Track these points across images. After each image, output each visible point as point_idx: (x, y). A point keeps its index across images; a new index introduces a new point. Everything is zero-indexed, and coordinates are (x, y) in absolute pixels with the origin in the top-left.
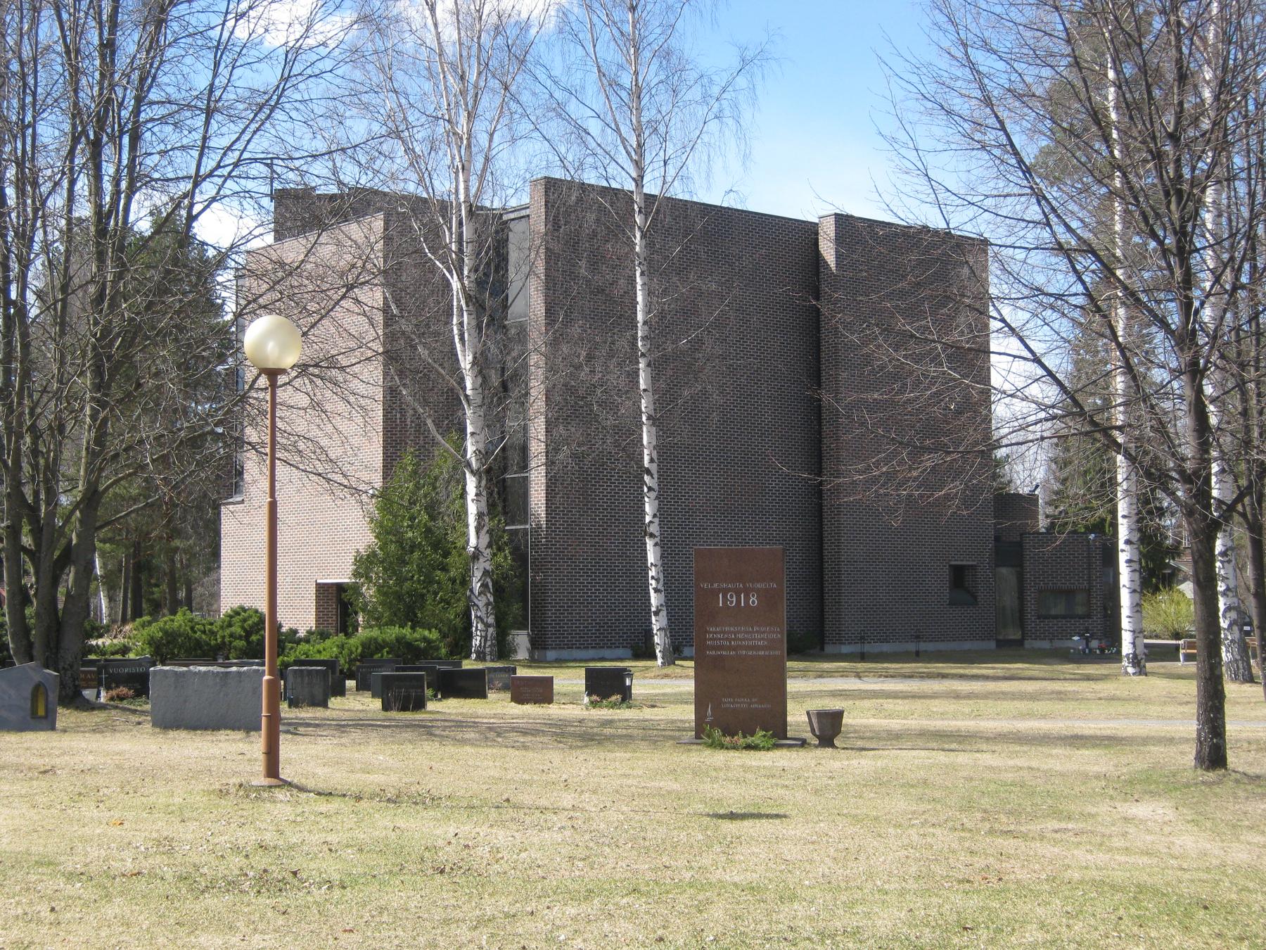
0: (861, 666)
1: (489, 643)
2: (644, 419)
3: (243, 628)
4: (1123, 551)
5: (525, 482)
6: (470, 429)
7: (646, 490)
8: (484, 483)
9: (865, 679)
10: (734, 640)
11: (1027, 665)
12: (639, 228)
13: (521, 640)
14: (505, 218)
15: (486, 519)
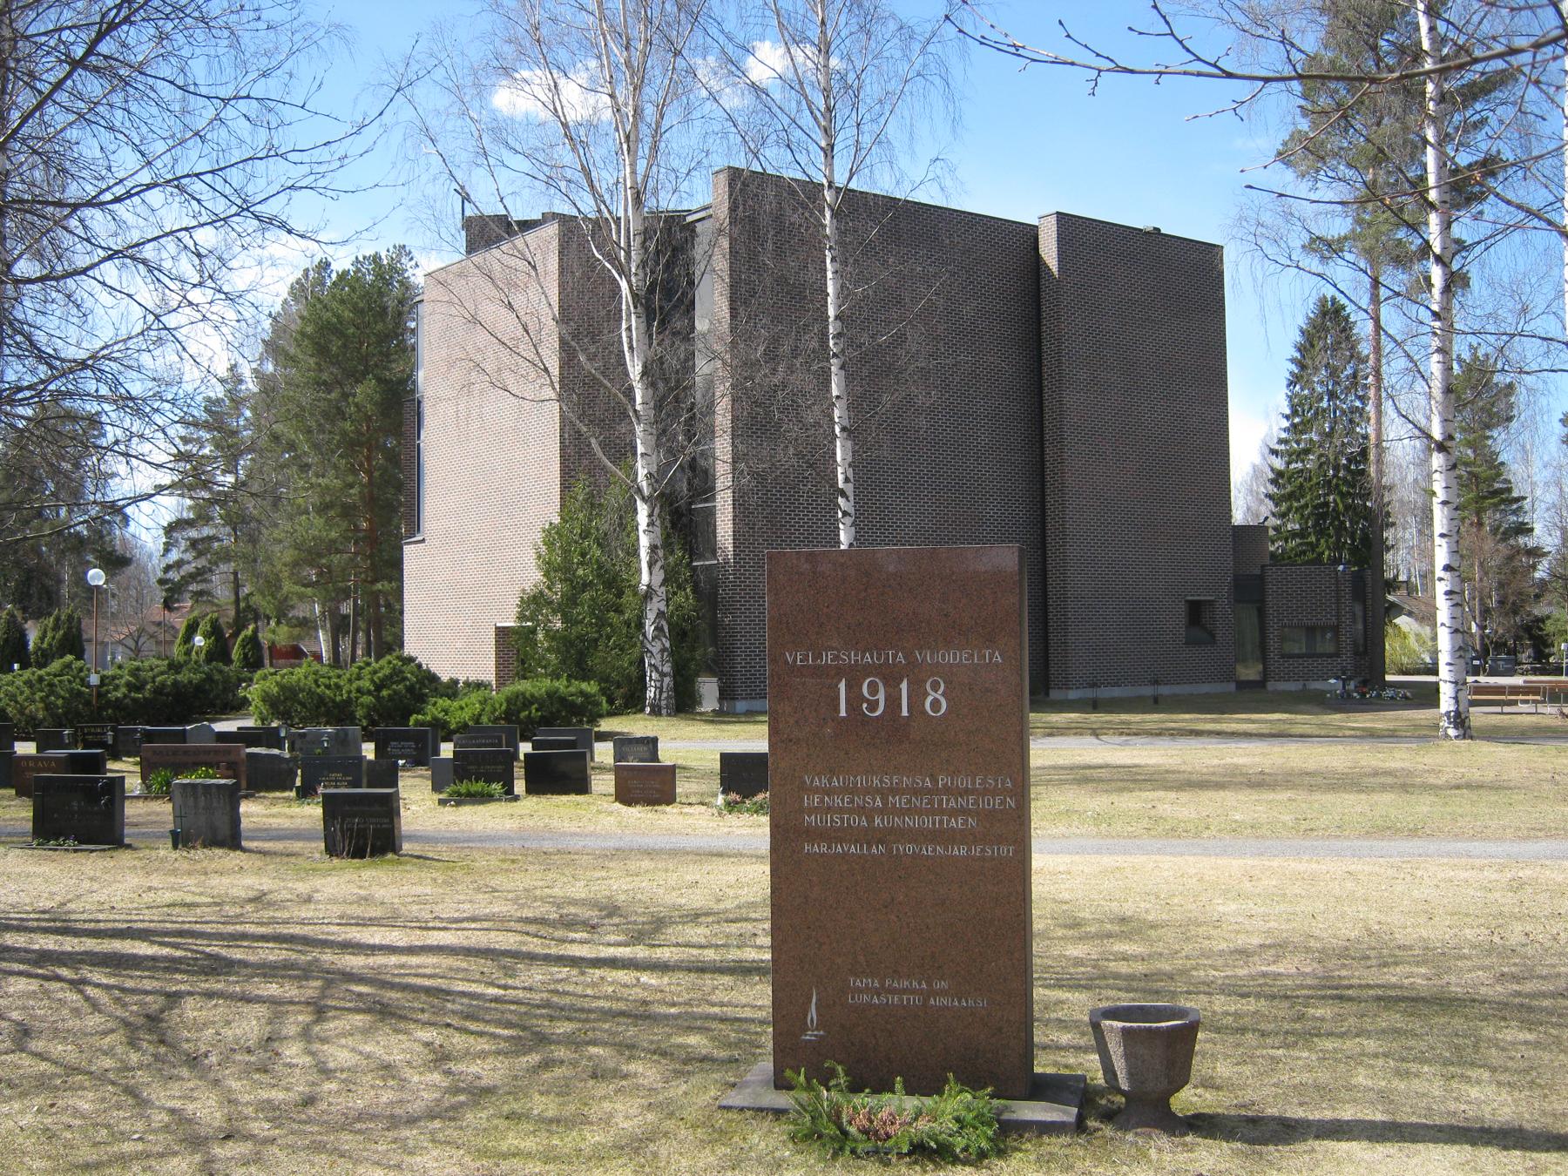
0: (1095, 718)
1: (664, 695)
2: (837, 430)
3: (372, 681)
4: (1441, 579)
5: (711, 513)
6: (640, 449)
7: (840, 515)
8: (657, 511)
9: (1102, 737)
10: (882, 812)
11: (1285, 716)
12: (829, 206)
13: (708, 689)
14: (690, 219)
15: (661, 553)
